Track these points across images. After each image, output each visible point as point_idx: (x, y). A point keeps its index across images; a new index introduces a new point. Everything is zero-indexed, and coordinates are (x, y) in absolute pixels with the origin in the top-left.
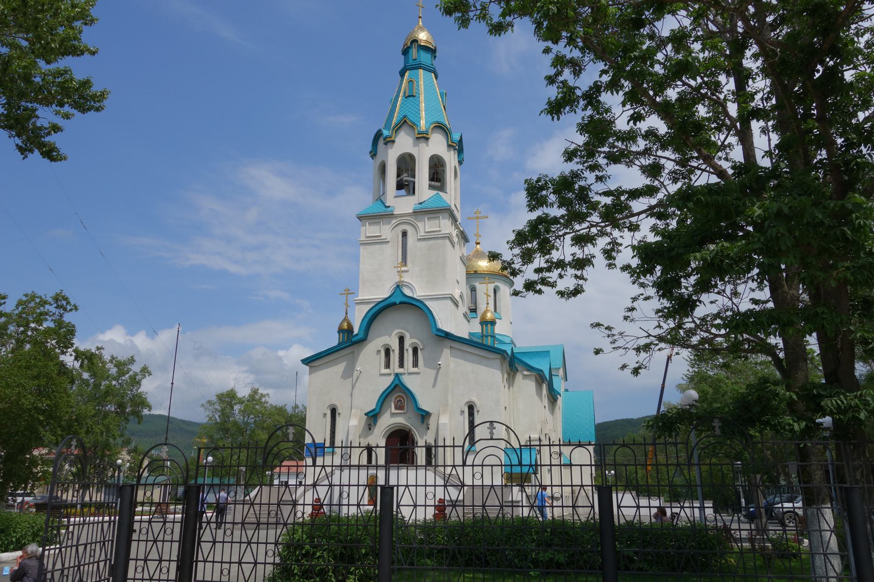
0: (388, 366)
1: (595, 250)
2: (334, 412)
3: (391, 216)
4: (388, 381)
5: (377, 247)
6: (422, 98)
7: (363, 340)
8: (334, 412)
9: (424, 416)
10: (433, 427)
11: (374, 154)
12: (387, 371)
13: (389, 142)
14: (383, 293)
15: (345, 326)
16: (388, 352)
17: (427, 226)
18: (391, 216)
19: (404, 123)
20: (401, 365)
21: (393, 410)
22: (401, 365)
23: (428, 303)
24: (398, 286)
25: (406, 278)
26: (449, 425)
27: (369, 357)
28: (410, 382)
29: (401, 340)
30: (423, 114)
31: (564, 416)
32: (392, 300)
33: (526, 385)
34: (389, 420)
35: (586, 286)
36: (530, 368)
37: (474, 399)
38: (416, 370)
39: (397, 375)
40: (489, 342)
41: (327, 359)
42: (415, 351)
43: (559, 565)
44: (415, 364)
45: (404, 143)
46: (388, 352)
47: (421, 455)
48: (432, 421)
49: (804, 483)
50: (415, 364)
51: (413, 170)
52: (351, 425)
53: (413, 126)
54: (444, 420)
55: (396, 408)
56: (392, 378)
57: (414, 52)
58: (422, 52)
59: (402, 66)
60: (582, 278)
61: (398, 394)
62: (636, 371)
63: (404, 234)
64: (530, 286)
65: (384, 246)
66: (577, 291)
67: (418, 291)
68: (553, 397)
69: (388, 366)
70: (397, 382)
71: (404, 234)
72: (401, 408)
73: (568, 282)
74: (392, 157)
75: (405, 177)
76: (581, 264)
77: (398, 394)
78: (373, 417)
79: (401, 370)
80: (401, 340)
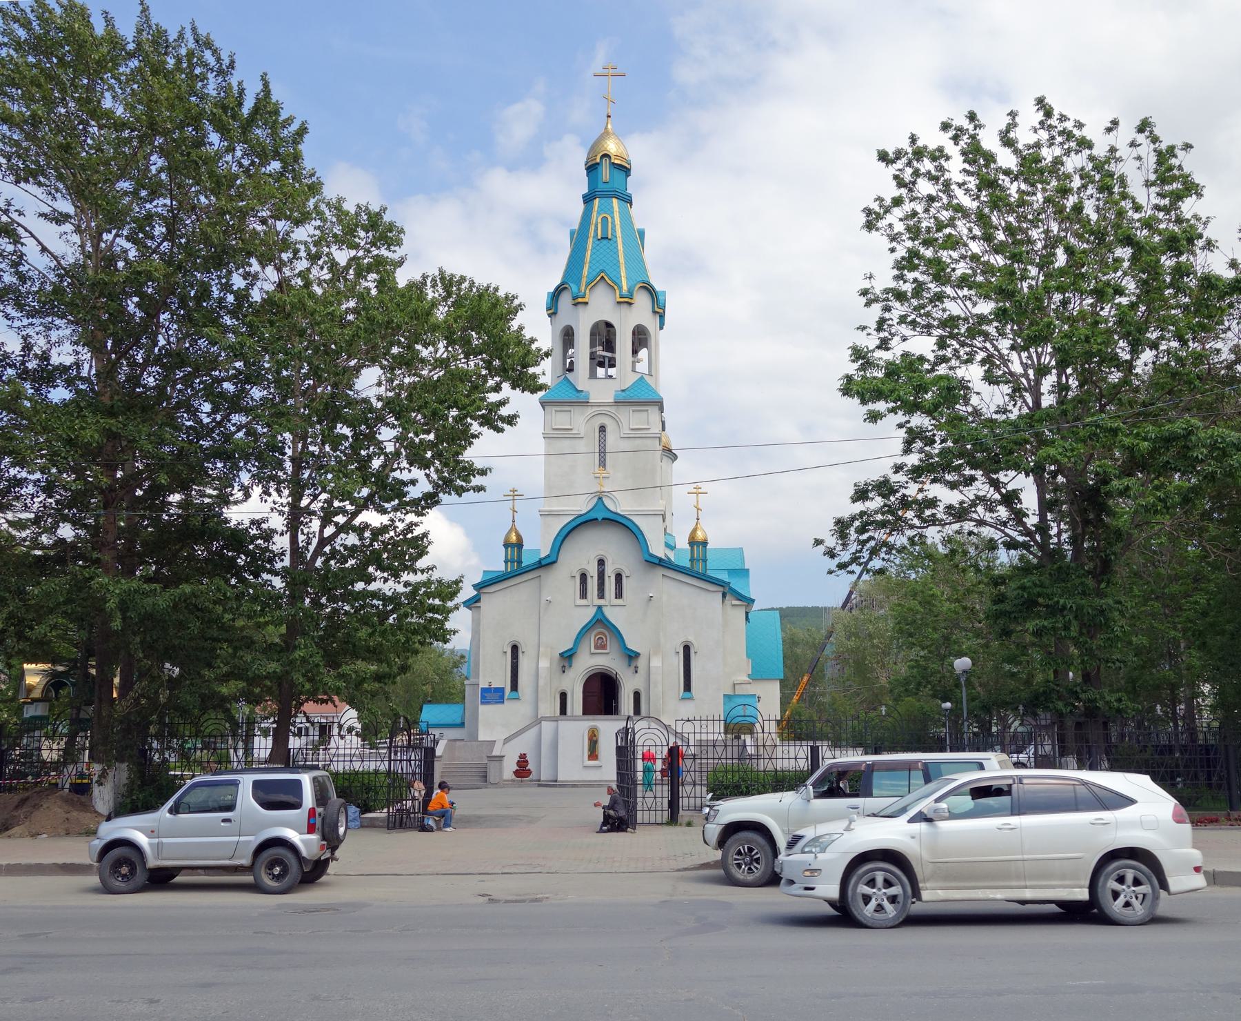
0: (584, 594)
2: (515, 649)
3: (586, 403)
4: (588, 614)
6: (619, 240)
8: (515, 649)
9: (632, 657)
10: (641, 670)
12: (584, 602)
14: (582, 506)
15: (514, 538)
16: (583, 577)
17: (632, 419)
18: (586, 403)
20: (601, 595)
21: (593, 650)
22: (601, 595)
26: (662, 668)
27: (561, 582)
28: (612, 615)
29: (601, 562)
34: (588, 662)
37: (691, 638)
38: (619, 601)
39: (600, 607)
40: (699, 567)
42: (619, 577)
44: (619, 595)
45: (601, 307)
46: (583, 577)
48: (641, 663)
49: (967, 680)
50: (619, 595)
52: (538, 663)
53: (613, 286)
54: (656, 663)
55: (596, 647)
57: (605, 172)
63: (603, 429)
64: (842, 566)
65: (577, 441)
67: (622, 505)
69: (584, 594)
70: (599, 617)
71: (603, 429)
72: (604, 647)
78: (567, 658)
79: (601, 602)
80: (601, 562)
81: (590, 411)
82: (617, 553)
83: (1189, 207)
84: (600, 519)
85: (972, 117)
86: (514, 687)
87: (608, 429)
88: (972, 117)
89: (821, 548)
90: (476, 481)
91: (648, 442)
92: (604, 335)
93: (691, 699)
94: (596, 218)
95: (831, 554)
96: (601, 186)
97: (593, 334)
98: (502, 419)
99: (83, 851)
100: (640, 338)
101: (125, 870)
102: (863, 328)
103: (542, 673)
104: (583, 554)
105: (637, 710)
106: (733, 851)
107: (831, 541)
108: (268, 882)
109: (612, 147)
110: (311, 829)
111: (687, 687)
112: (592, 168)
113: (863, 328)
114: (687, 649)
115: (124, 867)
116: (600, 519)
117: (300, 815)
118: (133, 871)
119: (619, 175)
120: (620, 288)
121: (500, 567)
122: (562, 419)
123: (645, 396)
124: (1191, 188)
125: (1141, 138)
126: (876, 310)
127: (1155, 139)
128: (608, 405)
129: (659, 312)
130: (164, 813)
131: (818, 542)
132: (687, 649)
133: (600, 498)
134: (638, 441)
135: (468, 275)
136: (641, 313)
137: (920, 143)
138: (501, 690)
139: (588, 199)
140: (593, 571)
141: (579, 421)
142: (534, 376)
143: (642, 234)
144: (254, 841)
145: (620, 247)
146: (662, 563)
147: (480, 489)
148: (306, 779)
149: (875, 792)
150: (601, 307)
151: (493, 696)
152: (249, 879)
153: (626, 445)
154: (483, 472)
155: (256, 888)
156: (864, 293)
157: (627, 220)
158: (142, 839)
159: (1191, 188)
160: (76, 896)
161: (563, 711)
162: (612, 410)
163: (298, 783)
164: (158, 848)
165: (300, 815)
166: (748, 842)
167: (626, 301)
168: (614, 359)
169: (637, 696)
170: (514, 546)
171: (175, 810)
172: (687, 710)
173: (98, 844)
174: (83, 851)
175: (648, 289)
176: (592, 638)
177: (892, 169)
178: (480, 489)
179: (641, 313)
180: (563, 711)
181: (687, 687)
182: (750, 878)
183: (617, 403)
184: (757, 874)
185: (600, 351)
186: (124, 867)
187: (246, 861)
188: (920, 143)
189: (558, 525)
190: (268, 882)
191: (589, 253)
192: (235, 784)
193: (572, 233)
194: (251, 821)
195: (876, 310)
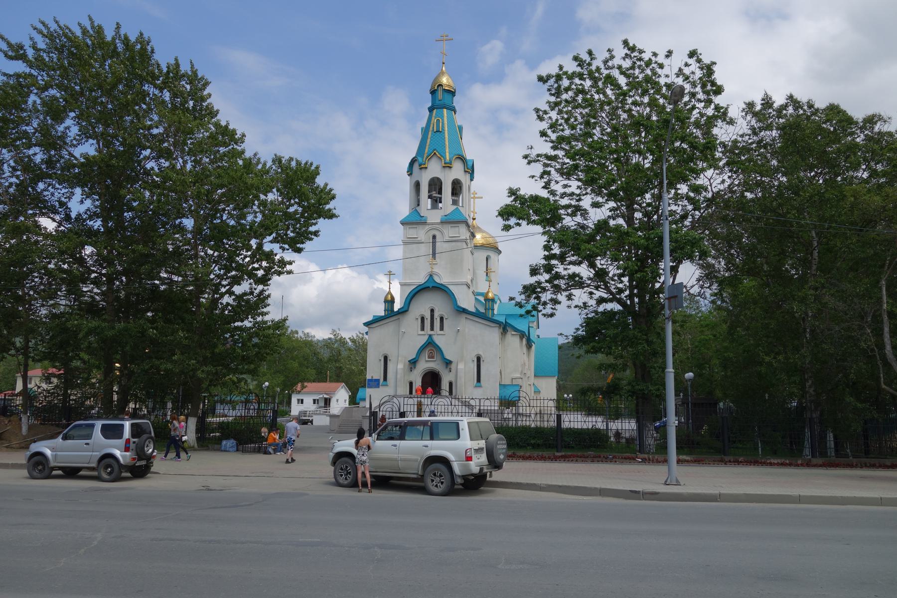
0: (423, 329)
1: (562, 297)
2: (386, 358)
3: (425, 223)
4: (423, 340)
5: (414, 245)
7: (403, 311)
8: (386, 358)
9: (448, 363)
11: (410, 172)
12: (422, 333)
13: (423, 168)
14: (421, 279)
15: (389, 298)
16: (423, 319)
17: (450, 232)
18: (425, 223)
19: (433, 155)
20: (432, 329)
22: (432, 329)
23: (451, 287)
24: (431, 276)
25: (436, 270)
26: (464, 369)
27: (410, 323)
28: (439, 340)
29: (432, 311)
30: (447, 150)
31: (536, 357)
32: (427, 285)
33: (513, 340)
34: (425, 365)
35: (557, 313)
36: (516, 330)
37: (481, 353)
38: (442, 332)
39: (430, 336)
41: (381, 323)
42: (442, 319)
43: (538, 445)
44: (442, 328)
45: (434, 169)
46: (423, 319)
47: (445, 386)
48: (453, 366)
50: (442, 328)
51: (441, 189)
52: (398, 367)
54: (461, 366)
56: (426, 338)
57: (440, 94)
58: (446, 94)
59: (430, 105)
60: (554, 309)
61: (430, 346)
62: (578, 357)
63: (434, 237)
64: (528, 312)
66: (552, 315)
67: (443, 279)
68: (529, 346)
69: (423, 329)
71: (434, 237)
72: (433, 357)
73: (548, 310)
74: (425, 179)
75: (435, 194)
76: (555, 302)
77: (430, 346)
78: (413, 363)
79: (432, 333)
80: (432, 311)
81: (427, 227)
82: (441, 307)
83: (718, 100)
84: (431, 287)
85: (590, 53)
86: (385, 379)
87: (437, 237)
88: (590, 53)
89: (513, 302)
90: (288, 267)
91: (459, 244)
92: (436, 185)
93: (480, 386)
94: (434, 120)
95: (520, 305)
96: (437, 102)
97: (430, 185)
98: (311, 233)
99: (21, 458)
100: (457, 188)
101: (40, 467)
102: (533, 177)
103: (400, 372)
104: (422, 307)
105: (451, 392)
106: (338, 467)
107: (520, 298)
108: (105, 476)
109: (445, 80)
110: (127, 449)
111: (479, 380)
112: (433, 92)
113: (533, 177)
114: (479, 359)
115: (39, 466)
116: (431, 287)
117: (121, 442)
118: (44, 468)
119: (448, 96)
120: (445, 159)
121: (383, 314)
122: (412, 233)
123: (456, 218)
124: (719, 90)
125: (692, 61)
126: (538, 168)
127: (699, 61)
128: (437, 224)
129: (470, 171)
130: (59, 440)
131: (511, 299)
132: (479, 359)
133: (431, 276)
134: (454, 244)
135: (294, 156)
136: (457, 172)
137: (564, 70)
138: (378, 380)
139: (431, 110)
140: (428, 316)
141: (422, 234)
142: (330, 210)
143: (461, 128)
144: (98, 454)
145: (447, 136)
146: (464, 311)
147: (290, 272)
148: (127, 425)
149: (441, 437)
150: (434, 169)
151: (375, 383)
152: (95, 473)
153: (447, 246)
154: (290, 263)
155: (98, 478)
156: (526, 157)
157: (452, 121)
158: (48, 452)
159: (719, 90)
160: (19, 478)
161: (411, 392)
162: (439, 226)
163: (122, 426)
164: (55, 457)
165: (121, 442)
166: (346, 463)
167: (448, 166)
168: (441, 198)
169: (451, 384)
170: (389, 301)
171: (65, 438)
172: (478, 393)
173: (29, 453)
174: (21, 458)
175: (462, 158)
176: (426, 354)
177: (547, 86)
178: (290, 272)
179: (457, 172)
180: (411, 392)
181: (479, 380)
182: (346, 482)
183: (442, 222)
184: (349, 480)
185: (435, 194)
186: (39, 466)
187: (94, 465)
188: (564, 70)
189: (409, 289)
190: (105, 476)
191: (429, 140)
192: (93, 426)
193: (422, 129)
194: (99, 443)
195: (538, 168)
